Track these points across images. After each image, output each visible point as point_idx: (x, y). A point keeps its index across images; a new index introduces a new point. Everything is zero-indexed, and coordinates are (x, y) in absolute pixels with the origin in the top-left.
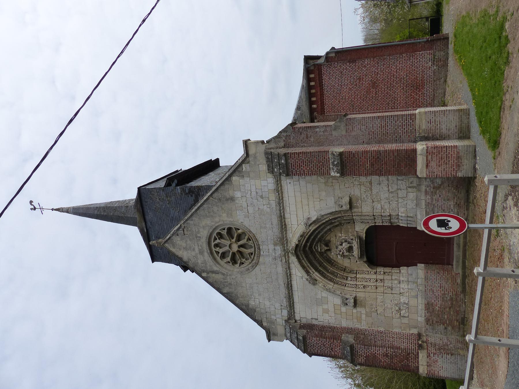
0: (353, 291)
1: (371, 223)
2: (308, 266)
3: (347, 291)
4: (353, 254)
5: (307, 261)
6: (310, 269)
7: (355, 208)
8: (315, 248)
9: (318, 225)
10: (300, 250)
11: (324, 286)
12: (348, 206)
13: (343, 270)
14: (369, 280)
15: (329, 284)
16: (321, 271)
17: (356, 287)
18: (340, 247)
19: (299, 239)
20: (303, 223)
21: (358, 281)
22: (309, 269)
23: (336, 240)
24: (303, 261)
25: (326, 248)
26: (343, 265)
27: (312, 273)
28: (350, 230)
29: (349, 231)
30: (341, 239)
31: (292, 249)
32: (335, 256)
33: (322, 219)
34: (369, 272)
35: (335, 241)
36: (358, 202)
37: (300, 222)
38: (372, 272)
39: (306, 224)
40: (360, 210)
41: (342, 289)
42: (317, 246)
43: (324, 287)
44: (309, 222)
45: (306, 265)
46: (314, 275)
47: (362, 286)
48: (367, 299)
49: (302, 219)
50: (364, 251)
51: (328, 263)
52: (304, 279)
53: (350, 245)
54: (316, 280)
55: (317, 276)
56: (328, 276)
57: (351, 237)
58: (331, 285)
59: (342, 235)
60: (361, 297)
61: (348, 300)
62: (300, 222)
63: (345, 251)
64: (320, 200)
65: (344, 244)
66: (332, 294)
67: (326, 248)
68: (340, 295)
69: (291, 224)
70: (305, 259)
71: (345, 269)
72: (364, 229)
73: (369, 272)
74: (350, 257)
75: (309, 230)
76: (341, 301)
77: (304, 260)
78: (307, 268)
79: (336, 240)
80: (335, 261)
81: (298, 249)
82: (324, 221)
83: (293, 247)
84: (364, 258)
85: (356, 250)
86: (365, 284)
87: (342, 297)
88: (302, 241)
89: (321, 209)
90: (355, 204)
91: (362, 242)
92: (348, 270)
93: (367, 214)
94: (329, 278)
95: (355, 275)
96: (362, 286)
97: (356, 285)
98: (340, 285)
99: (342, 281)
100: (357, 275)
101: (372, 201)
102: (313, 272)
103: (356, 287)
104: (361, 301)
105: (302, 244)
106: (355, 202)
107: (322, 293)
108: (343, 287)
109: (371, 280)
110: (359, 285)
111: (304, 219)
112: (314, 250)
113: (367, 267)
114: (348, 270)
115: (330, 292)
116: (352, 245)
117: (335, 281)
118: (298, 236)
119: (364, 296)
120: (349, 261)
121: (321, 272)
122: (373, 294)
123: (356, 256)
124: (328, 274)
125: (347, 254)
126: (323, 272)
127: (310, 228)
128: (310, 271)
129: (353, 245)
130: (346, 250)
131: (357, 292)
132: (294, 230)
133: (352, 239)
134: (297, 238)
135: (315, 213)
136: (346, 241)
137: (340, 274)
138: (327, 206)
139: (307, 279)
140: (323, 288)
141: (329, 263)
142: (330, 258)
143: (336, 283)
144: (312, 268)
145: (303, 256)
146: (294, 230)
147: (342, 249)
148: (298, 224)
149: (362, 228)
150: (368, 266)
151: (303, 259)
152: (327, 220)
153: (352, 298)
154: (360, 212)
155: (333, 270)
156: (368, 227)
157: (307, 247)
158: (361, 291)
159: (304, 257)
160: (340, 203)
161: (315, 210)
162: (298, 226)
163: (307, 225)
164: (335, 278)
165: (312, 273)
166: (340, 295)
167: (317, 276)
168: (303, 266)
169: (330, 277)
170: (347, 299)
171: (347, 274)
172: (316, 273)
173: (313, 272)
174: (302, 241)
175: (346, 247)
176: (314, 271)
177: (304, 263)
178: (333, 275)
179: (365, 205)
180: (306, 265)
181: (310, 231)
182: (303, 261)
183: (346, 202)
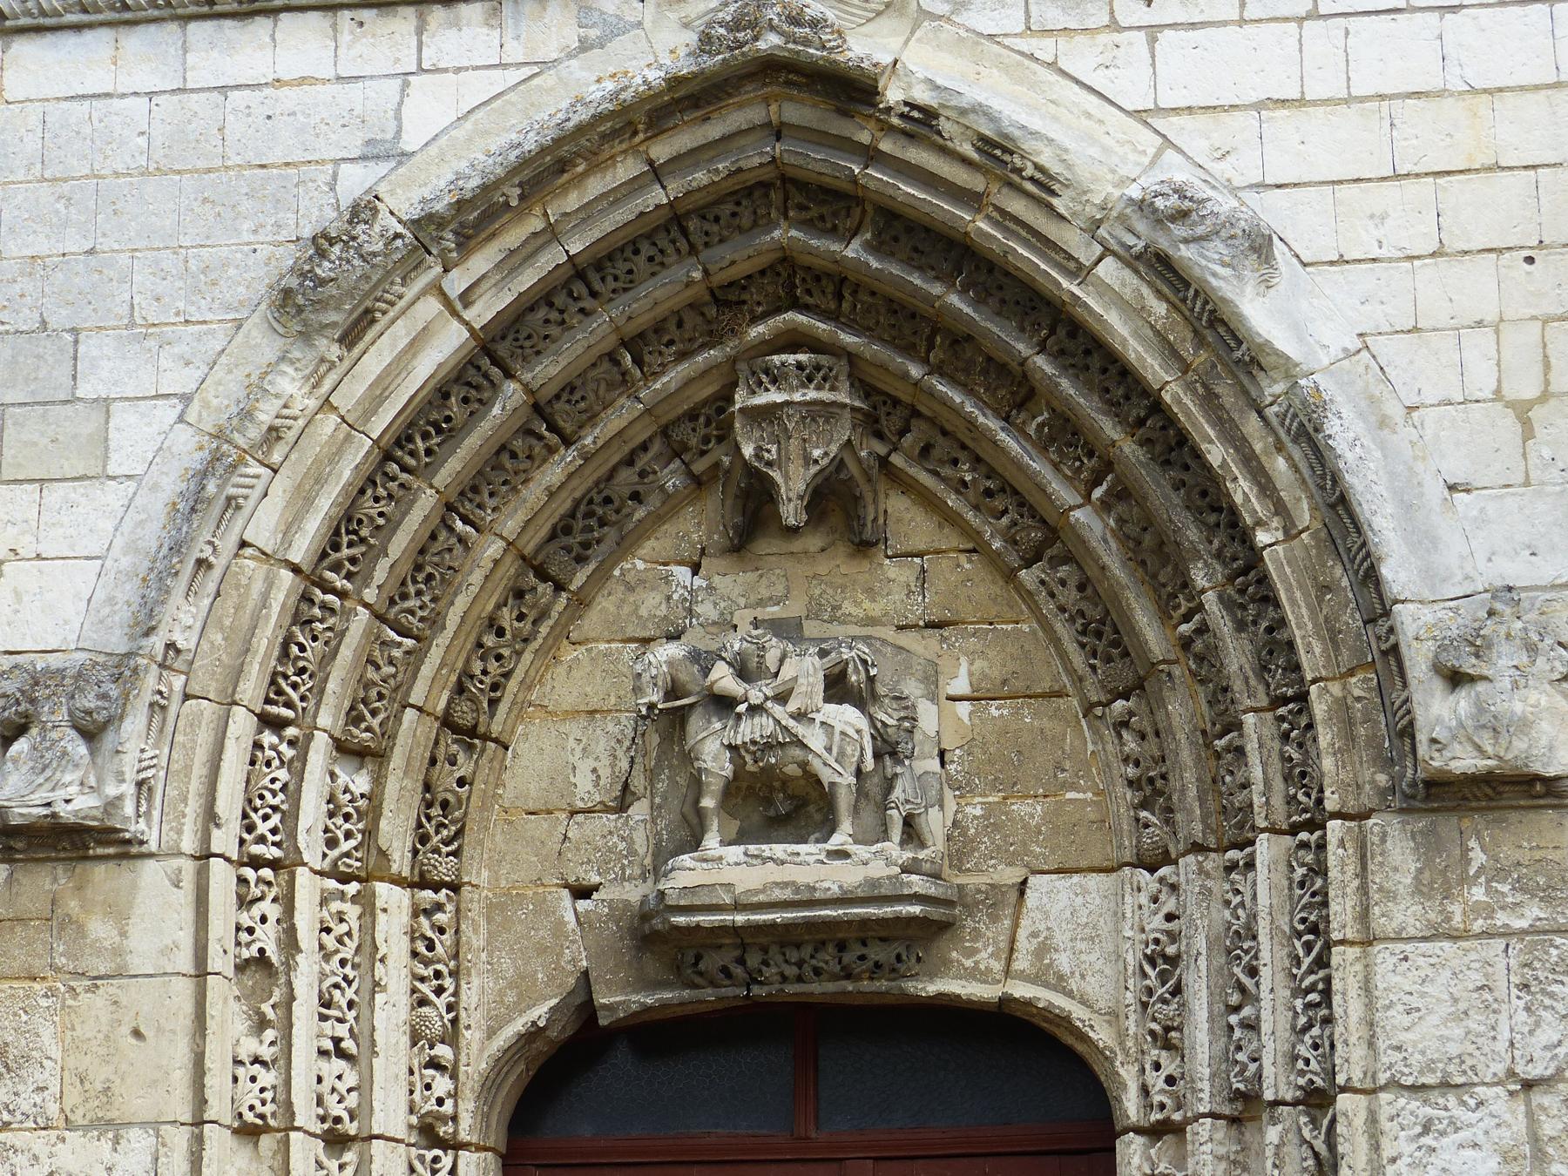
0: (210, 818)
1: (1157, 1081)
2: (551, 234)
3: (205, 738)
4: (711, 842)
5: (623, 215)
6: (513, 261)
7: (1428, 846)
8: (793, 341)
9: (1152, 367)
10: (778, 132)
11: (274, 434)
12: (1465, 762)
13: (464, 714)
14: (348, 1044)
15: (303, 500)
16: (477, 404)
17: (256, 863)
18: (806, 671)
19: (945, 126)
20: (1181, 174)
21: (324, 902)
22: (514, 237)
23: (889, 633)
24: (627, 169)
25: (792, 484)
26: (520, 709)
27: (456, 283)
28: (1029, 810)
29: (1011, 787)
30: (912, 688)
31: (815, 24)
32: (651, 603)
33: (1251, 426)
34: (443, 1051)
35: (875, 608)
36: (1520, 887)
37: (1192, 134)
38: (442, 1085)
39: (1182, 215)
40: (1404, 913)
41: (237, 674)
42: (808, 376)
43: (254, 433)
44: (1217, 248)
45: (572, 201)
46: (432, 306)
47: (268, 939)
48: (94, 1005)
49: (1243, 169)
50: (752, 979)
51: (563, 505)
52: (355, 181)
53: (844, 801)
54: (350, 338)
55: (415, 345)
56: (403, 498)
57: (935, 823)
58: (289, 529)
59: (964, 709)
60: (119, 914)
61: (80, 749)
62: (1198, 147)
63: (750, 730)
64: (1522, 412)
65: (846, 716)
66: (153, 534)
67: (792, 484)
68: (157, 643)
69: (1152, 32)
70: (657, 196)
71: (470, 735)
72: (1059, 984)
73: (443, 1051)
74: (639, 810)
75: (1085, 253)
76: (55, 661)
77: (634, 186)
78: (521, 213)
79: (889, 633)
80: (581, 602)
81: (796, 112)
82: (1216, 453)
83: (579, 100)
84: (627, 987)
85: (772, 873)
86: (306, 977)
87: (123, 669)
88: (917, 155)
89: (1395, 410)
90: (1478, 857)
91: (877, 953)
92: (464, 768)
93: (1348, 1006)
94: (369, 507)
95: (400, 863)
96: (268, 939)
97: (274, 865)
98: (285, 653)
99: (331, 686)
100: (398, 881)
101: (1534, 1071)
102: (467, 298)
103: (256, 863)
104: (55, 919)
105: (871, 156)
106: (1507, 853)
107: (167, 412)
108: (252, 689)
109: (339, 1065)
110: (287, 902)
111: (1234, 191)
112: (758, 331)
113: (518, 1026)
114: (464, 768)
115: (195, 503)
116: (846, 826)
117: (328, 589)
118: (996, 104)
119: (137, 964)
120: (584, 788)
121: (454, 406)
122: (180, 1078)
123: (687, 873)
124: (426, 503)
125: (714, 758)
126: (448, 432)
127: (1109, 270)
128: (481, 262)
129: (838, 840)
130: (769, 746)
131: (189, 867)
132: (1081, 59)
133: (912, 832)
134: (973, 94)
135: (1337, 337)
136: (888, 748)
137: (415, 658)
138: (1436, 491)
139: (363, 211)
140: (247, 415)
141: (561, 530)
142: (625, 545)
143: (307, 598)
144: (527, 279)
145: (701, 177)
146: (1081, 59)
147: (782, 698)
148: (1159, 111)
149: (1063, 962)
150: (533, 1034)
151: (657, 173)
152: (1242, 490)
153: (113, 804)
154: (1364, 916)
155: (477, 578)
156: (1102, 1035)
157: (807, 225)
158: (213, 932)
159: (676, 187)
160: (1504, 660)
161: (1376, 343)
162: (1137, 114)
163: (1179, 230)
164: (370, 595)
165: (456, 283)
166: (157, 643)
167: (415, 345)
168: (562, 166)
169: (393, 525)
170: (91, 733)
171: (420, 763)
172: (449, 342)
173: (467, 298)
174: (917, 155)
175: (815, 739)
176: (483, 312)
177: (596, 186)
178: (405, 568)
179: (1477, 978)
180: (572, 201)
181: (1080, 272)
182: (627, 169)
183: (1524, 725)
